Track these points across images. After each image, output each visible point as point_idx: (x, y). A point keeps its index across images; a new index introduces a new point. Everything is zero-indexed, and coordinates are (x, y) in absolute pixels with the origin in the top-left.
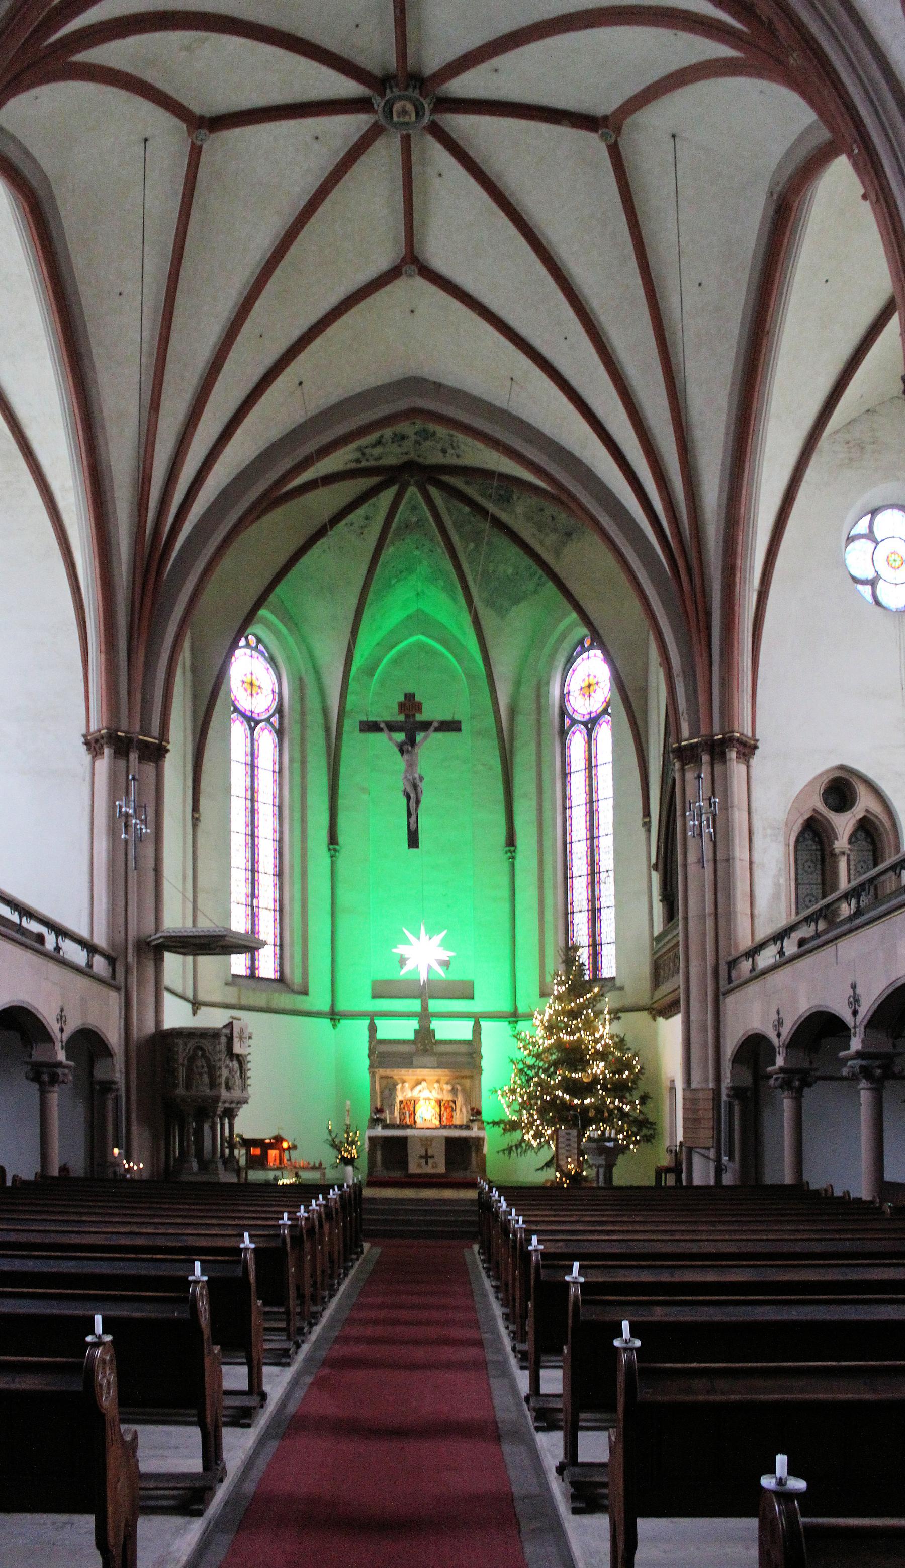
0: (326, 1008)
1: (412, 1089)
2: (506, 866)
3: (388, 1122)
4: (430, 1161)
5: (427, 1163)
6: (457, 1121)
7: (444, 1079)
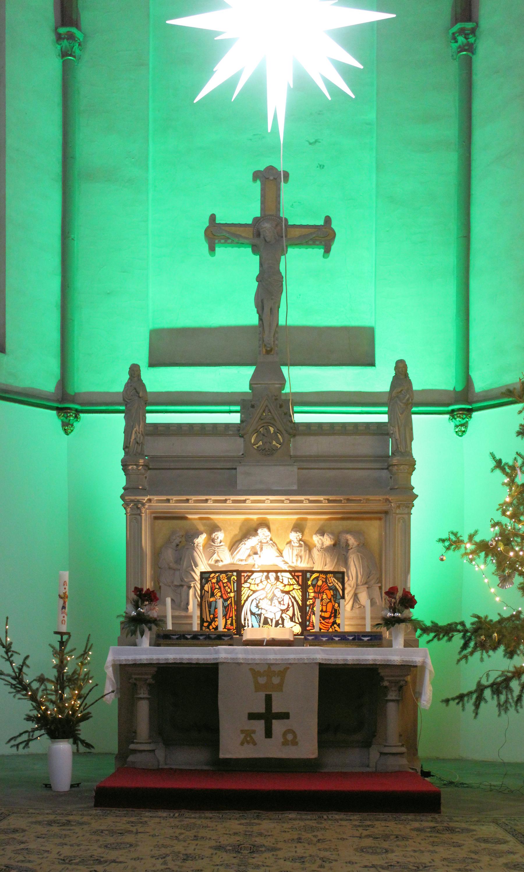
0: (49, 385)
1: (234, 546)
2: (452, 71)
3: (170, 627)
4: (277, 726)
5: (269, 734)
6: (347, 623)
7: (314, 520)
